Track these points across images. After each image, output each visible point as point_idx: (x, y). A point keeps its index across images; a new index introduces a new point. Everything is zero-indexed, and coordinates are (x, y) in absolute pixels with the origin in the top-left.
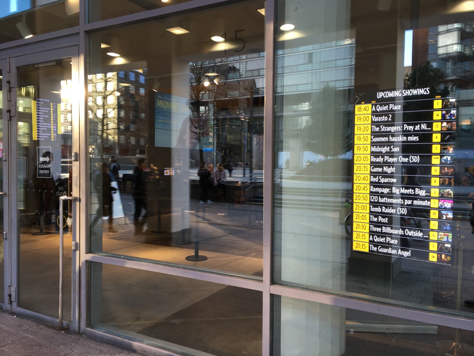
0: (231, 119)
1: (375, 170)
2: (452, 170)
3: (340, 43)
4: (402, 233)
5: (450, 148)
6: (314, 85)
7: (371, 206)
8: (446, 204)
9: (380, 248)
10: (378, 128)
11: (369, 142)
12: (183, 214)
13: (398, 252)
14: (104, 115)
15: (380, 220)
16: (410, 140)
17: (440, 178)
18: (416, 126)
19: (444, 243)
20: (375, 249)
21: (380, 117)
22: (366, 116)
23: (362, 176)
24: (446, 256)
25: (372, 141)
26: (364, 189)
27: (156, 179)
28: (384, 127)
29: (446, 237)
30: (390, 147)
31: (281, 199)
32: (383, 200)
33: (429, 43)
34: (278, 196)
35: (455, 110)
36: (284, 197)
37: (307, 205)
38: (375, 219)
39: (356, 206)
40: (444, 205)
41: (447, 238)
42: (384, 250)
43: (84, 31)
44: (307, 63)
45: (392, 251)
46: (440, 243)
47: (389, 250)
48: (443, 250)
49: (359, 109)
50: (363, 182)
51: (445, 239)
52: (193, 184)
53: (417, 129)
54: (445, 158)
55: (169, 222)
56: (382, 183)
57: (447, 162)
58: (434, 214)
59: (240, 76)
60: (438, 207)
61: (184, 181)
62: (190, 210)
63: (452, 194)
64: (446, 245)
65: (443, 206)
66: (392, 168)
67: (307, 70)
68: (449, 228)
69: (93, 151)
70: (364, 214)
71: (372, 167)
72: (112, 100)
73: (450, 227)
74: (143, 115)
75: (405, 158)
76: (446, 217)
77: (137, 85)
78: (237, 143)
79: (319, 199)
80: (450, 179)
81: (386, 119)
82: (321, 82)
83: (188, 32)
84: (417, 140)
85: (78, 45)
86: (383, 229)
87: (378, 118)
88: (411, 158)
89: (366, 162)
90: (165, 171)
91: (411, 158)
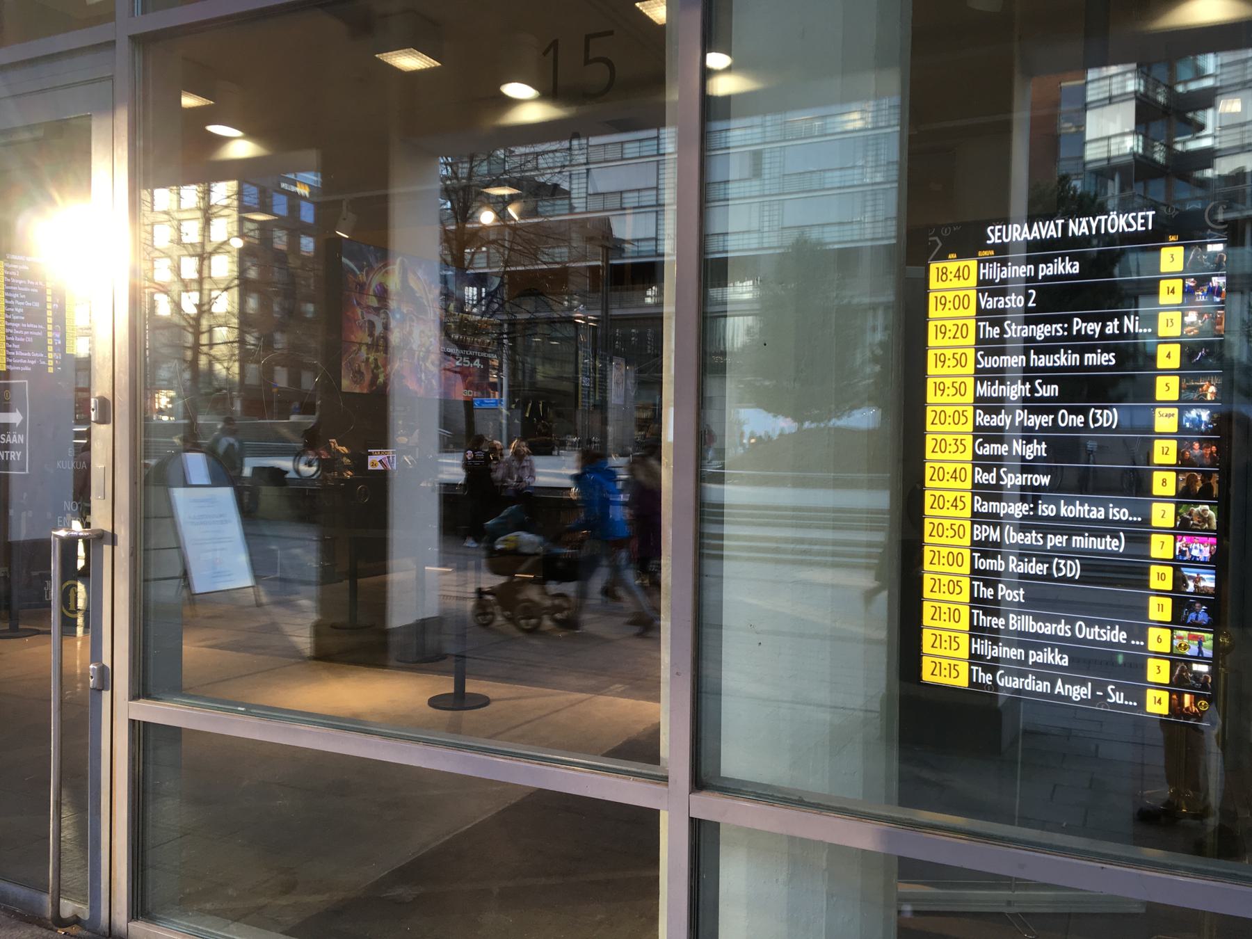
0: (551, 322)
1: (988, 449)
2: (1214, 448)
3: (834, 128)
4: (1066, 632)
5: (1208, 387)
6: (765, 235)
7: (976, 555)
8: (1196, 548)
9: (1001, 674)
10: (997, 328)
11: (970, 369)
12: (421, 577)
13: (1053, 686)
14: (199, 306)
15: (1003, 596)
16: (1095, 364)
17: (1178, 472)
18: (1108, 323)
19: (1188, 661)
20: (987, 678)
21: (1002, 298)
22: (961, 294)
23: (949, 468)
24: (1197, 698)
25: (978, 366)
26: (956, 506)
27: (346, 480)
28: (1014, 327)
29: (1197, 642)
30: (1032, 384)
31: (721, 537)
32: (1029, 538)
33: (1063, 131)
34: (711, 529)
35: (1222, 275)
36: (728, 530)
37: (793, 552)
38: (989, 593)
39: (932, 553)
40: (1190, 550)
41: (1200, 648)
42: (1013, 681)
43: (129, 37)
44: (747, 177)
45: (1036, 684)
46: (1177, 660)
47: (1030, 680)
48: (1188, 681)
49: (940, 274)
50: (953, 484)
51: (1193, 650)
52: (449, 495)
53: (1111, 332)
54: (1193, 414)
55: (380, 597)
56: (1009, 487)
57: (1199, 427)
58: (1161, 577)
59: (571, 209)
60: (1171, 557)
61: (422, 485)
62: (440, 566)
63: (1215, 520)
64: (1196, 667)
65: (1188, 553)
66: (1037, 444)
67: (747, 195)
68: (1203, 617)
69: (170, 406)
70: (955, 579)
71: (980, 443)
72: (224, 267)
73: (1206, 615)
74: (310, 308)
75: (1074, 417)
76: (1196, 587)
77: (295, 228)
78: (567, 386)
79: (829, 535)
80: (1207, 475)
81: (1020, 303)
82: (783, 228)
83: (438, 64)
84: (1110, 363)
85: (111, 78)
86: (1011, 622)
87: (996, 299)
88: (1095, 414)
89: (960, 428)
90: (370, 459)
91: (1095, 414)
